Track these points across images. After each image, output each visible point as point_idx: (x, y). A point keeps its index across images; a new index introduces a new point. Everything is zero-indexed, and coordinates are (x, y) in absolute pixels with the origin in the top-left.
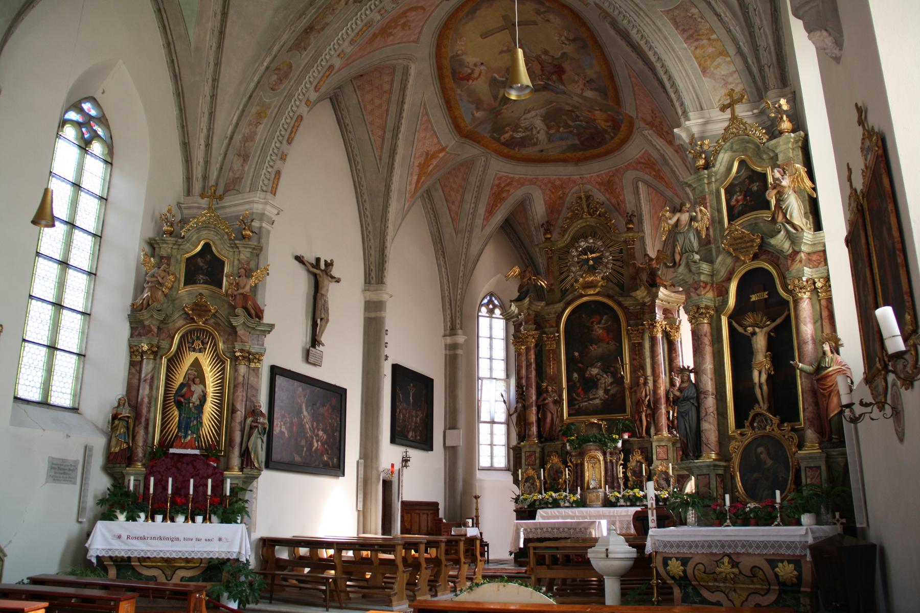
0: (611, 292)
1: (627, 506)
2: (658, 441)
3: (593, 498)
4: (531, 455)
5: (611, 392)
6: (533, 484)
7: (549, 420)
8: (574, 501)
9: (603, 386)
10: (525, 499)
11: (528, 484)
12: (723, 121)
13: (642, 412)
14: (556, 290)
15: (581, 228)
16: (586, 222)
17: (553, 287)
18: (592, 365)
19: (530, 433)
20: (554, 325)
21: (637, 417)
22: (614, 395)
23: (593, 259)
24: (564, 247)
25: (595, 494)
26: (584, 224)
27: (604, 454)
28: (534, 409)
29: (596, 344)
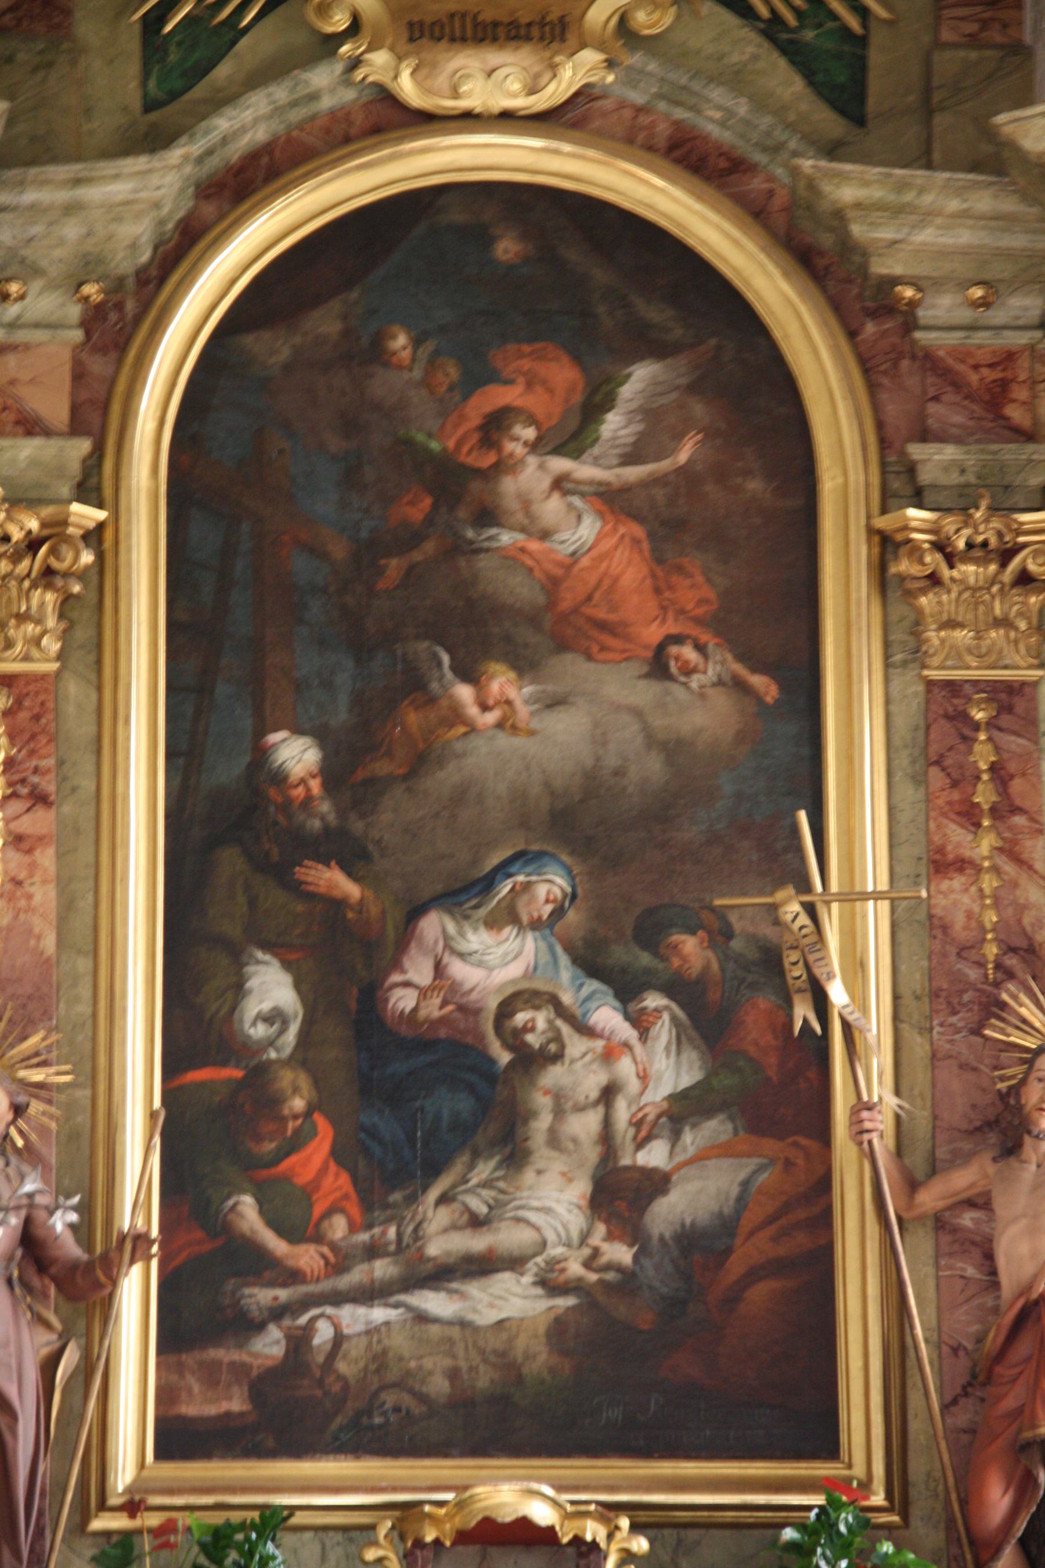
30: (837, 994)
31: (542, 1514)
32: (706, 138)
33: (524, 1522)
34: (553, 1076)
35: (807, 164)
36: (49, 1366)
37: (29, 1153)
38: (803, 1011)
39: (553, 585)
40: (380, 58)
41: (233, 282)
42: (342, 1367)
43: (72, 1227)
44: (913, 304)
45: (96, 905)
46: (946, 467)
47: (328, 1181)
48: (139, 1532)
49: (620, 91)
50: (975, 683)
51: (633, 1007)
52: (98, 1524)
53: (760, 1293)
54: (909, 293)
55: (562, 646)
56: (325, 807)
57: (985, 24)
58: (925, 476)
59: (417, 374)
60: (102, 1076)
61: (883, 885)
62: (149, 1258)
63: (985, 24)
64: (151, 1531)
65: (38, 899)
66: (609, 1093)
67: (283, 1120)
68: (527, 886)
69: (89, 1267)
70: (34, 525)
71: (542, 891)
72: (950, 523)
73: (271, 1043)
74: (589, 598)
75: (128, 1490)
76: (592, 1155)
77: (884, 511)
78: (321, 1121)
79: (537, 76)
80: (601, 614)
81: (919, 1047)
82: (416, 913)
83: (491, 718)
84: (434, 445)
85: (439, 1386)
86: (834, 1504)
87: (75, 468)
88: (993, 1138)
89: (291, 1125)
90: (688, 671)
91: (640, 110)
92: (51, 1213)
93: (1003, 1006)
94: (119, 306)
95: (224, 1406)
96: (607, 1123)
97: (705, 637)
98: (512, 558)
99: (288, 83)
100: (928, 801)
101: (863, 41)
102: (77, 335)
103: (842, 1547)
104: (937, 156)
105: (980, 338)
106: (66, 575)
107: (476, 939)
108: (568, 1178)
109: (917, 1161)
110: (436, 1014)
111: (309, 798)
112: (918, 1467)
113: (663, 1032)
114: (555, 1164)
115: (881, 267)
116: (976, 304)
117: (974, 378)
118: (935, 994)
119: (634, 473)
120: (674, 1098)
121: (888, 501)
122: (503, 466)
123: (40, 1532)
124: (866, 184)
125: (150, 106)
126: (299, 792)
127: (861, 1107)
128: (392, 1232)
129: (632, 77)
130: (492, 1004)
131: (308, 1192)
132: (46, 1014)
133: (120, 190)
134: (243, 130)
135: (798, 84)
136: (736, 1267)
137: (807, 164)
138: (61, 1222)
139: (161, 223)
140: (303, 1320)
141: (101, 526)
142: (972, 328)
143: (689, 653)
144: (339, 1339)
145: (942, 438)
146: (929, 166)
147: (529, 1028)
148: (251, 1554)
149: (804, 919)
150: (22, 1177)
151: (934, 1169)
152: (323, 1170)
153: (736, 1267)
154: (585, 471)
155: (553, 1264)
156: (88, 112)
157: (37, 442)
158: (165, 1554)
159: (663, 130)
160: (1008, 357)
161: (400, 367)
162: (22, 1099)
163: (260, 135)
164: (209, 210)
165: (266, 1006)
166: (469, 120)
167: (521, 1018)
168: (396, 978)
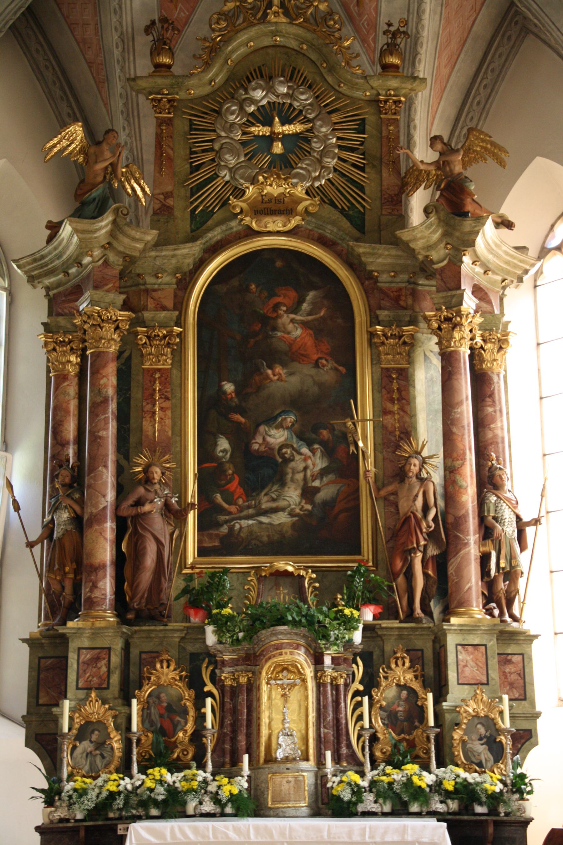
0: (329, 232)
1: (385, 814)
2: (463, 630)
3: (285, 787)
4: (96, 659)
5: (321, 496)
6: (100, 745)
7: (150, 560)
8: (233, 798)
9: (300, 476)
10: (82, 793)
11: (85, 746)
12: (106, 226)
13: (414, 550)
14: (177, 213)
15: (255, 51)
16: (274, 34)
17: (170, 202)
18: (271, 421)
19: (97, 594)
20: (169, 303)
21: (399, 564)
22: (327, 505)
23: (285, 139)
24: (205, 97)
25: (290, 776)
26: (267, 42)
27: (318, 660)
28: (109, 526)
29: (284, 365)
30: (361, 444)
31: (290, 569)
32: (326, 237)
33: (286, 571)
34: (292, 464)
35: (351, 243)
36: (172, 535)
37: (166, 484)
38: (352, 448)
39: (290, 345)
40: (248, 219)
41: (212, 273)
42: (242, 534)
43: (176, 501)
44: (377, 277)
45: (181, 424)
46: (386, 316)
47: (238, 490)
48: (194, 573)
49: (305, 226)
50: (393, 369)
51: (311, 448)
52: (184, 572)
53: (342, 516)
54: (376, 274)
55: (293, 360)
56: (236, 400)
57: (393, 210)
58: (381, 318)
59: (257, 294)
60: (183, 465)
61: (371, 418)
62: (195, 509)
63: (393, 210)
64: (197, 573)
65: (167, 423)
66: (305, 469)
67: (226, 476)
68: (285, 419)
69: (181, 511)
70: (165, 332)
71: (289, 420)
72: (387, 330)
73: (223, 457)
74: (300, 348)
75: (192, 564)
76: (301, 483)
77: (371, 326)
78: (236, 476)
79: (285, 223)
80: (303, 352)
81: (380, 456)
82: (258, 426)
83: (276, 378)
84: (262, 312)
85: (265, 539)
86: (360, 566)
87: (175, 318)
88: (398, 478)
89: (229, 477)
90: (324, 366)
91: (310, 230)
92: (171, 498)
93: (400, 446)
94: (185, 279)
95: (214, 544)
96: (305, 476)
97: (329, 359)
98: (280, 339)
99: (225, 225)
100: (382, 397)
101: (364, 214)
102: (175, 286)
103: (362, 575)
104: (382, 241)
105: (393, 285)
106: (173, 344)
107: (273, 432)
108: (296, 489)
109: (380, 484)
110: (263, 450)
111: (232, 397)
112: (380, 556)
113: (318, 454)
114: (293, 486)
115: (369, 268)
116: (392, 277)
117: (392, 294)
118: (384, 444)
119: (310, 318)
120: (321, 470)
121: (372, 324)
122: (279, 317)
123: (170, 574)
124: (365, 248)
125: (192, 232)
126: (230, 396)
127: (366, 471)
128: (253, 502)
129: (308, 223)
130: (277, 447)
131: (233, 493)
132: (169, 451)
133: (185, 251)
134: (215, 236)
135: (349, 224)
136: (336, 509)
137: (351, 243)
138: (174, 500)
139: (195, 259)
140: (232, 523)
141: (181, 332)
142: (392, 282)
143: (324, 362)
144: (241, 528)
145: (384, 309)
146: (380, 243)
147: (286, 453)
148: (221, 579)
149: (352, 426)
150: (164, 490)
151: (384, 486)
152: (237, 488)
153: (336, 509)
154: (298, 318)
155: (293, 510)
156: (177, 233)
157: (165, 312)
158: (200, 579)
159: (316, 235)
160: (400, 289)
161: (253, 293)
162: (164, 471)
163: (219, 237)
164: (206, 256)
165: (222, 448)
166: (269, 233)
167: (284, 451)
168: (254, 441)
